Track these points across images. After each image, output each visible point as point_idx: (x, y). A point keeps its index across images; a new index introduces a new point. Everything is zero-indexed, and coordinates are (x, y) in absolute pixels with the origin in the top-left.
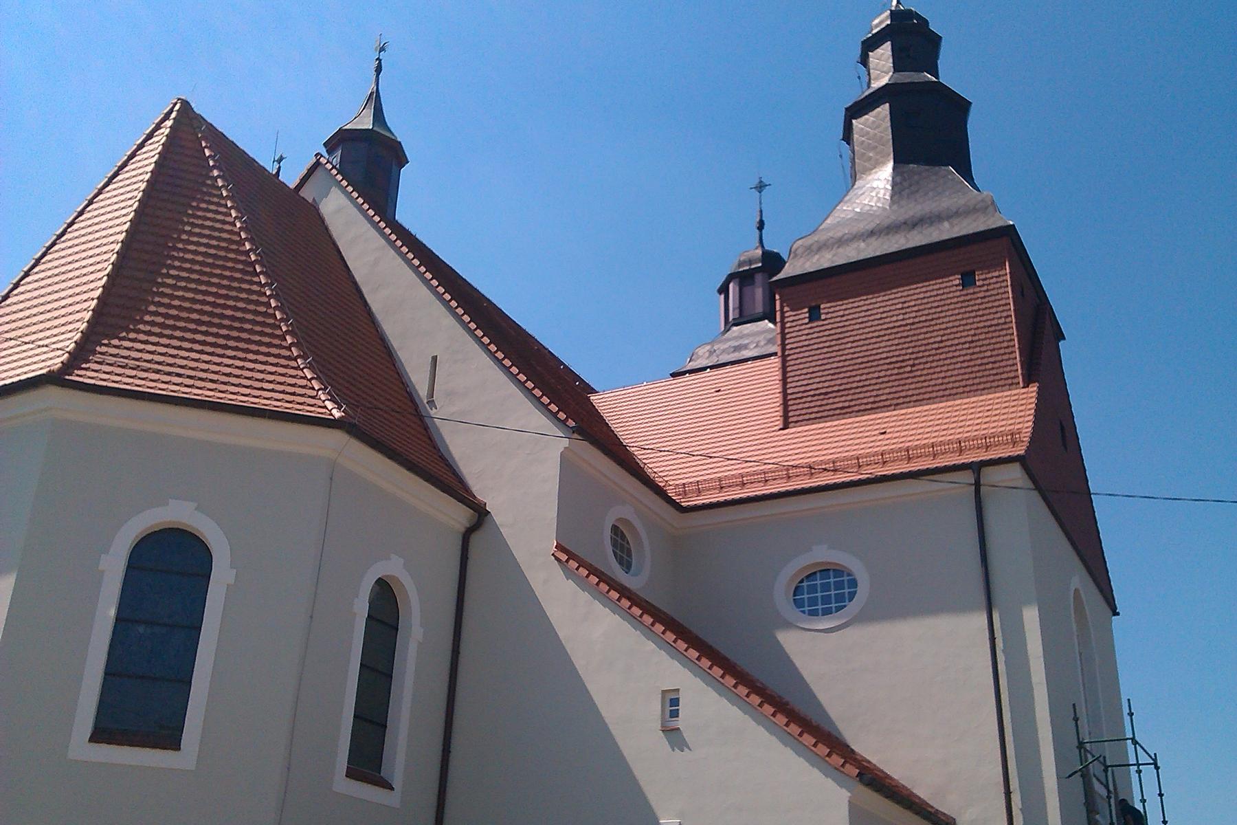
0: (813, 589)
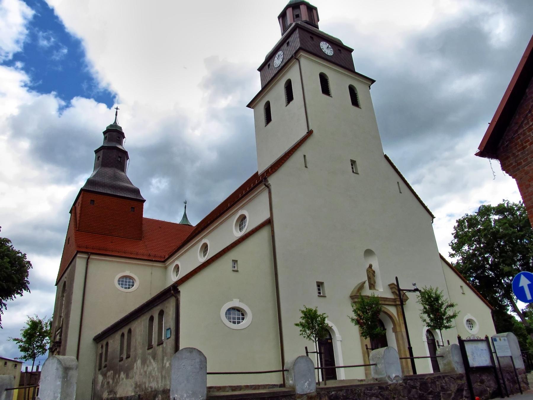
0: (123, 281)
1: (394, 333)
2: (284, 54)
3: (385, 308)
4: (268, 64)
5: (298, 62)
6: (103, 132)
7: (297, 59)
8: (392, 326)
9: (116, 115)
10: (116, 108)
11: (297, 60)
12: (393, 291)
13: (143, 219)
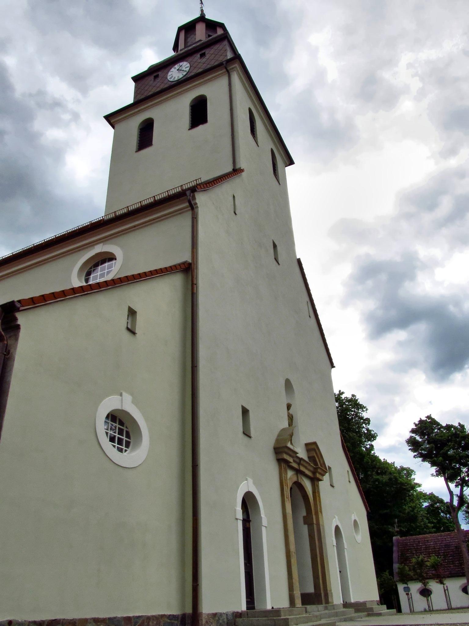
1: (306, 526)
3: (303, 480)
5: (227, 75)
8: (304, 513)
11: (227, 72)
12: (311, 455)
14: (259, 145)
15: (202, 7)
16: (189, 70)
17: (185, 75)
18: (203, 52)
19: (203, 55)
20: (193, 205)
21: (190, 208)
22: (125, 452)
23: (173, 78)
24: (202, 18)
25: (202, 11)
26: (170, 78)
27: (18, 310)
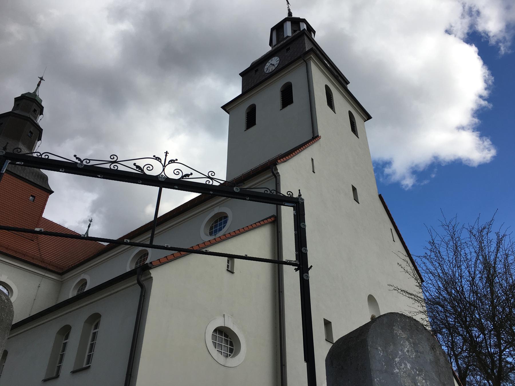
2: (280, 60)
4: (288, 47)
6: (15, 98)
7: (305, 61)
9: (39, 85)
10: (40, 78)
13: (42, 218)
14: (336, 112)
15: (289, 7)
16: (279, 63)
17: (277, 67)
18: (288, 47)
19: (288, 49)
20: (275, 175)
21: (274, 177)
22: (229, 356)
23: (268, 71)
24: (290, 18)
25: (289, 10)
26: (266, 71)
27: (151, 268)
